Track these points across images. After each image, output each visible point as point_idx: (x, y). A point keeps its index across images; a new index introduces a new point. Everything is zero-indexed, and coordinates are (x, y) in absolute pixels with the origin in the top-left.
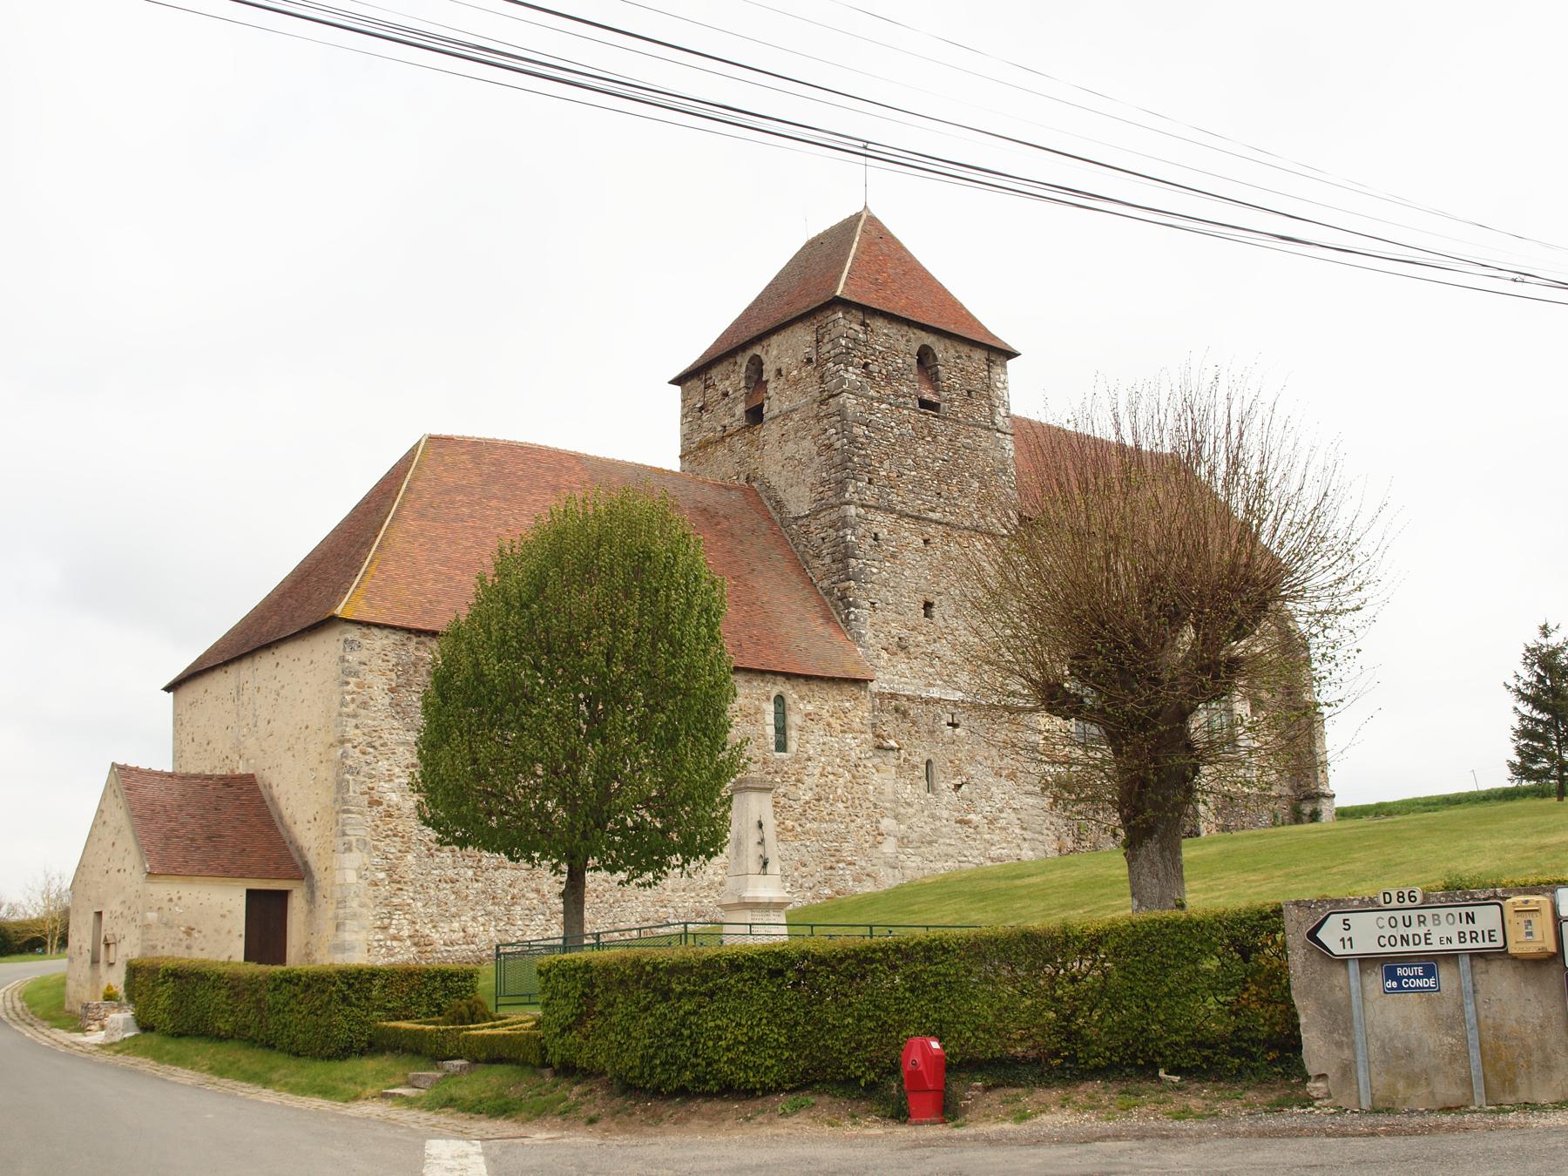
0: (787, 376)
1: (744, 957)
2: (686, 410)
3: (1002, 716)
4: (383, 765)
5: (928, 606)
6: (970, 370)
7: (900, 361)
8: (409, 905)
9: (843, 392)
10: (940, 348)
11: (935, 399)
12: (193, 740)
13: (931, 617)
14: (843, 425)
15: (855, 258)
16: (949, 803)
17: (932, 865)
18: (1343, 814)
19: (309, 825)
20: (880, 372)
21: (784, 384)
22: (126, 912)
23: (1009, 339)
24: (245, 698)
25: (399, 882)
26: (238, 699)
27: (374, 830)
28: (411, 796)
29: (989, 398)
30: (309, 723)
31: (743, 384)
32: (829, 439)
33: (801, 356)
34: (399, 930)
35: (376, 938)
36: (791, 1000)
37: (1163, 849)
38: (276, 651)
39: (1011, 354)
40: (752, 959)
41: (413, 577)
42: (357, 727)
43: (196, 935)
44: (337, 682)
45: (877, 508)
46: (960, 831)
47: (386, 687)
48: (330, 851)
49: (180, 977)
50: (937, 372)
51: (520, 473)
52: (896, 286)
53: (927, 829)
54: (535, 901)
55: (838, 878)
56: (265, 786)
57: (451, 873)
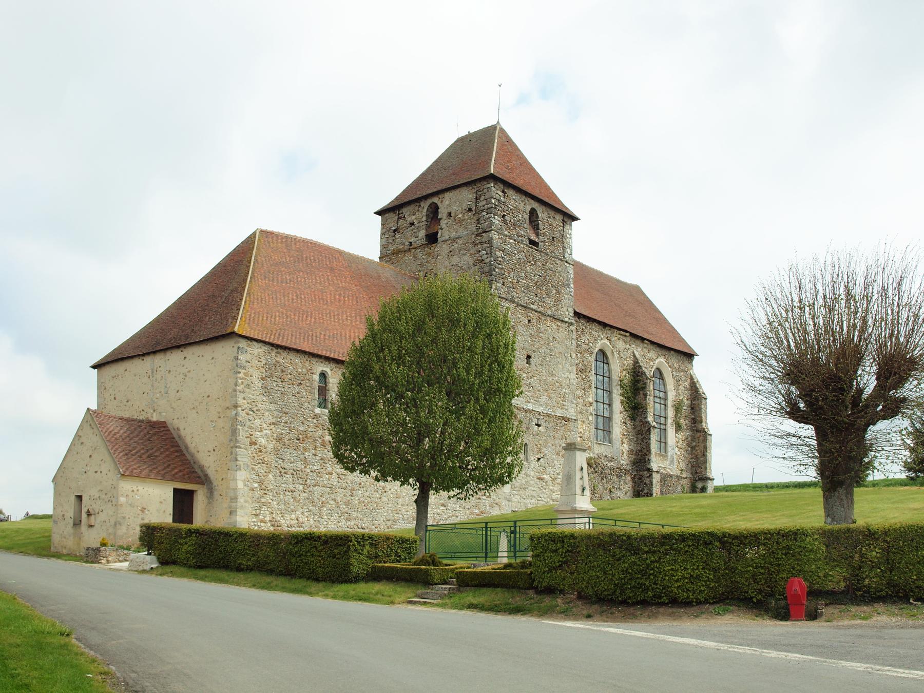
1: (689, 534)
2: (384, 230)
3: (561, 423)
5: (529, 357)
6: (554, 225)
7: (520, 216)
8: (270, 503)
9: (492, 230)
10: (542, 213)
11: (536, 240)
12: (115, 398)
13: (530, 364)
14: (491, 249)
15: (497, 152)
16: (534, 468)
18: (717, 489)
19: (209, 454)
20: (510, 221)
21: (453, 221)
22: (103, 496)
23: (575, 211)
24: (158, 376)
25: (265, 490)
26: (153, 377)
28: (272, 441)
29: (563, 243)
31: (424, 219)
32: (481, 257)
33: (465, 207)
34: (265, 517)
36: (717, 557)
40: (694, 535)
41: (269, 313)
42: (244, 399)
43: (147, 513)
44: (232, 371)
45: (506, 299)
46: (539, 483)
47: (260, 377)
48: (226, 469)
49: (200, 534)
50: (538, 224)
51: (312, 258)
52: (518, 171)
53: (523, 482)
54: (333, 506)
56: (174, 429)
57: (291, 487)
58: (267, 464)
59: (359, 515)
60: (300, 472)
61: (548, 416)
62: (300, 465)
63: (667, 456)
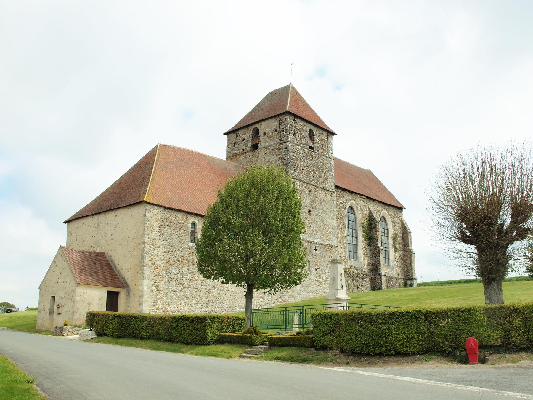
0: (267, 135)
2: (229, 143)
4: (156, 251)
5: (310, 211)
6: (323, 138)
7: (304, 133)
8: (162, 298)
10: (316, 131)
11: (313, 146)
12: (76, 240)
13: (310, 215)
14: (288, 152)
16: (314, 274)
17: (309, 294)
18: (419, 285)
19: (128, 270)
20: (298, 136)
22: (67, 296)
24: (101, 227)
25: (159, 291)
26: (98, 227)
27: (153, 273)
30: (130, 236)
31: (251, 136)
33: (273, 129)
34: (159, 307)
35: (152, 308)
37: (498, 285)
38: (116, 211)
39: (333, 134)
40: (409, 313)
42: (149, 238)
46: (316, 283)
47: (158, 226)
49: (120, 318)
50: (314, 138)
54: (199, 299)
55: (284, 297)
56: (109, 257)
57: (174, 288)
58: (161, 276)
59: (213, 304)
60: (180, 280)
61: (321, 245)
62: (180, 276)
63: (390, 266)
